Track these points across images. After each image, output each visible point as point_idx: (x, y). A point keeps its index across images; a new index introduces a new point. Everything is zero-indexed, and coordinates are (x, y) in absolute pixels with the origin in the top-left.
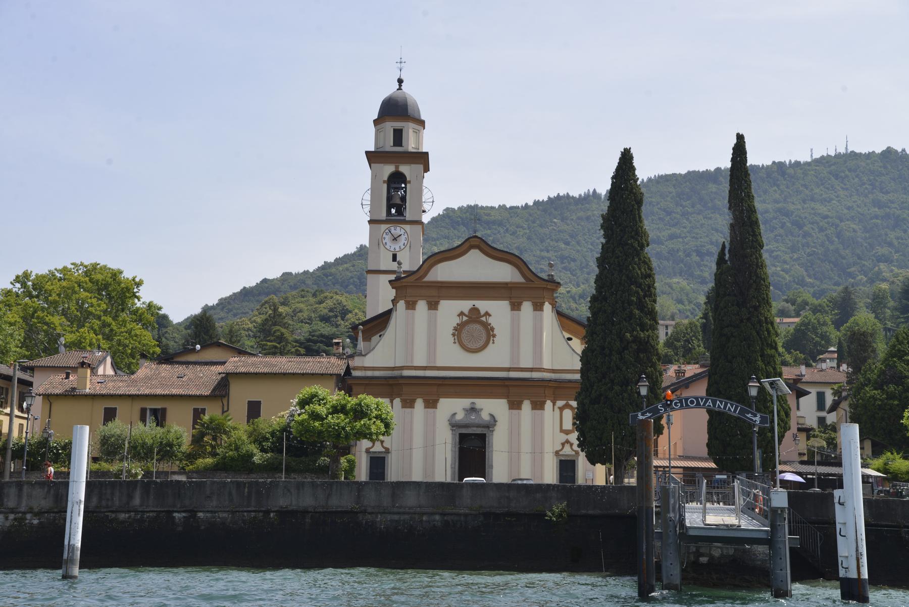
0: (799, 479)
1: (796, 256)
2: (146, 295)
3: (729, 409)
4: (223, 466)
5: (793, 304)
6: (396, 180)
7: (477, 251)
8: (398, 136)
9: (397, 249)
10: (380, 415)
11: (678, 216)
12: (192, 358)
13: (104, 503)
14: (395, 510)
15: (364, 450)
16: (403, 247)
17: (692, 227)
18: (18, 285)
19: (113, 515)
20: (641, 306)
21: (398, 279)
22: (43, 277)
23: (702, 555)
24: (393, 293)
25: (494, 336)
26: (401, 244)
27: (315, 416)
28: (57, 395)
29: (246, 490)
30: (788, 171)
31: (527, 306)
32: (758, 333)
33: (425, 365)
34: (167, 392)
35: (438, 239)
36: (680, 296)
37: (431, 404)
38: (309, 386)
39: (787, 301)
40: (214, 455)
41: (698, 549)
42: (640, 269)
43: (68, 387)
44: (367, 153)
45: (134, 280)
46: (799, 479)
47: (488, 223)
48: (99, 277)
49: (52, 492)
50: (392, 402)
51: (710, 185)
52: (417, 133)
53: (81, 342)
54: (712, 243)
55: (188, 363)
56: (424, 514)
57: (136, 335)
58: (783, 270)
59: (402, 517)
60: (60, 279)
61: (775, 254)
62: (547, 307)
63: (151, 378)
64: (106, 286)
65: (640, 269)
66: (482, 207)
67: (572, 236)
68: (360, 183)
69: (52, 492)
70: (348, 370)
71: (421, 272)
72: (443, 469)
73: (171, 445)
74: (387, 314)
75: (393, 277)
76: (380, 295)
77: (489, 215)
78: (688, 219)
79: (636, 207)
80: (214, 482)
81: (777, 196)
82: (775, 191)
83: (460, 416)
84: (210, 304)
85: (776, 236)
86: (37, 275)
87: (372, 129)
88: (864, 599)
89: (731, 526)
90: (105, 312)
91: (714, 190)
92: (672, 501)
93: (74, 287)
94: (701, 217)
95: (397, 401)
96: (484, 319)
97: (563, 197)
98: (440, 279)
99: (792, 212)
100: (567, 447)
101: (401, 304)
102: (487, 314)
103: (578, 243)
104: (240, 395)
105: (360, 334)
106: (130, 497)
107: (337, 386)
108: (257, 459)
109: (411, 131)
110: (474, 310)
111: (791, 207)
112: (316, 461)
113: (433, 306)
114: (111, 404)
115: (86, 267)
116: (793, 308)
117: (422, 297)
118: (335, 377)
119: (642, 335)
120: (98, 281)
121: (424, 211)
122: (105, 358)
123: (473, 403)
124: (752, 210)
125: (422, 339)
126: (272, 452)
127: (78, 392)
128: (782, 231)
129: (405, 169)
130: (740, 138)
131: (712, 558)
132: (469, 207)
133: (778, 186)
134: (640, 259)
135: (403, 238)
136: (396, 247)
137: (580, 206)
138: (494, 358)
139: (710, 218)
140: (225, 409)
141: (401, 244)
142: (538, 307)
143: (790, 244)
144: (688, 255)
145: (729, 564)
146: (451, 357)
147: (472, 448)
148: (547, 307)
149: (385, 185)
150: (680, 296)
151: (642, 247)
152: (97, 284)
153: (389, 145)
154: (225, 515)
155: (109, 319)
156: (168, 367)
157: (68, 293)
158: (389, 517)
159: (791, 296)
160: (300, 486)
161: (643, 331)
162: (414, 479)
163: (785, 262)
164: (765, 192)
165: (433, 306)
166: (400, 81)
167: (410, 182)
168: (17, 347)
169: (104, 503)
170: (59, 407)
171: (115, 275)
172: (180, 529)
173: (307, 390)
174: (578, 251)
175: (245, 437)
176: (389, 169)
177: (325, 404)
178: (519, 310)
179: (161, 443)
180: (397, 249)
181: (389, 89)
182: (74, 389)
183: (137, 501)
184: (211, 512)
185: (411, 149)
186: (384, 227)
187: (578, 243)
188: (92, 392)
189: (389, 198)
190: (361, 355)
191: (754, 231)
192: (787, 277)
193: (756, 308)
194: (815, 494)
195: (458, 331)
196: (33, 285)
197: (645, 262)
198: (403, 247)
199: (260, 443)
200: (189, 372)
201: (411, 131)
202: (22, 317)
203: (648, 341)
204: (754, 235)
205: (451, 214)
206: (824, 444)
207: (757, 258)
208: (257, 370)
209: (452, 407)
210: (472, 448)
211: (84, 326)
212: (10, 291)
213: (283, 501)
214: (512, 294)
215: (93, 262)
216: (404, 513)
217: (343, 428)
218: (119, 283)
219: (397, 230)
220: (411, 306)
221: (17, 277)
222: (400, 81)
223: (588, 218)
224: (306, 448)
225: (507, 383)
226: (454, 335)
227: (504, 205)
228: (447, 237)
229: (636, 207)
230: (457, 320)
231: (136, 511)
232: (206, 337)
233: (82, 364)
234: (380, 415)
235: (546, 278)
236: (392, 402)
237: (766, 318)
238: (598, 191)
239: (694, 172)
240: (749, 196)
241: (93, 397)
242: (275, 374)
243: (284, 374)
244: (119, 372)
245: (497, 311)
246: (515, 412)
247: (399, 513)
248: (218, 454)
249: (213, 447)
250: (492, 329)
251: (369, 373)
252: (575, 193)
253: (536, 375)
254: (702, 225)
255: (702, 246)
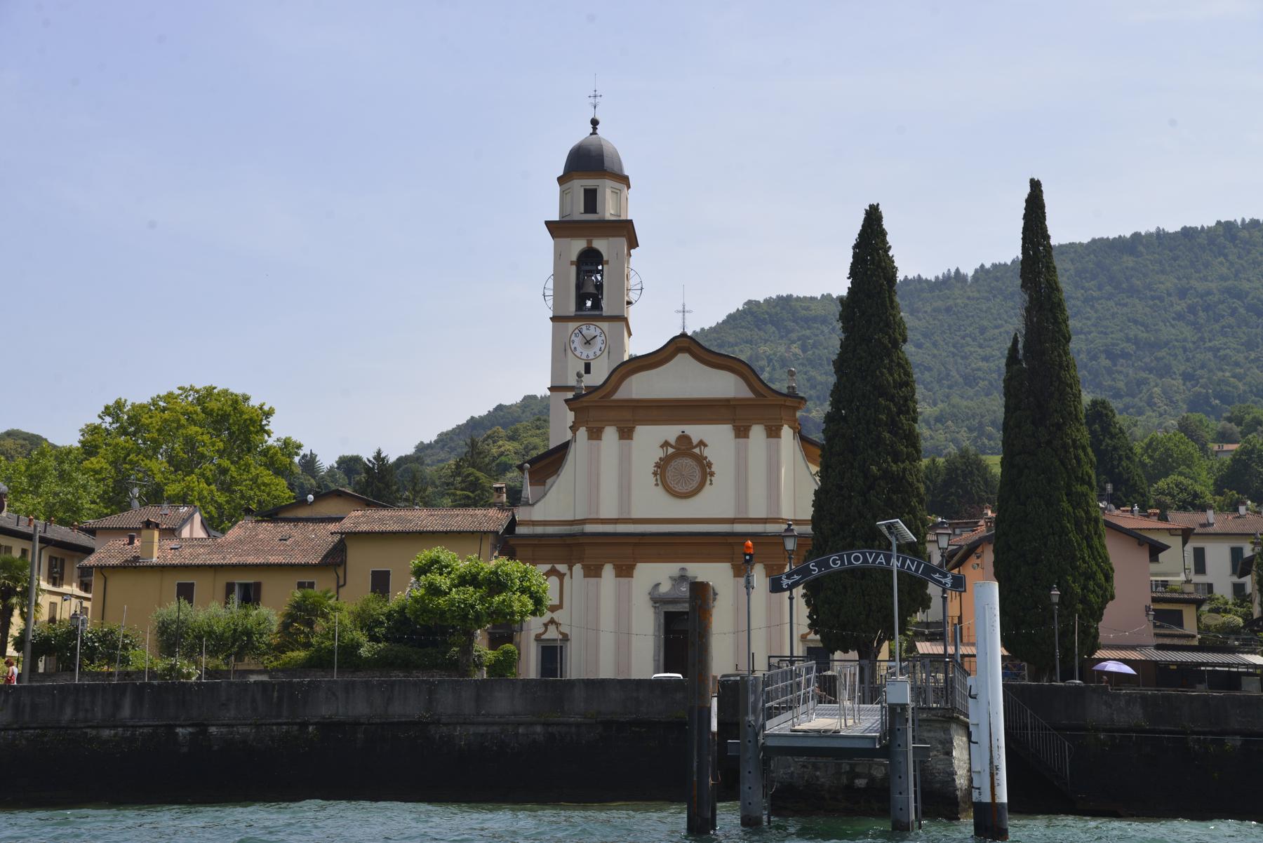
0: (1127, 669)
1: (1253, 355)
2: (278, 430)
3: (909, 567)
4: (320, 661)
5: (1239, 424)
6: (589, 261)
7: (687, 355)
8: (591, 198)
9: (592, 356)
10: (529, 588)
11: (1079, 303)
12: (303, 513)
13: (81, 715)
14: (481, 719)
15: (533, 636)
16: (598, 353)
17: (1099, 318)
18: (109, 419)
19: (94, 732)
20: (893, 426)
21: (576, 397)
22: (142, 407)
23: (859, 776)
24: (570, 416)
25: (712, 474)
26: (597, 349)
27: (434, 590)
28: (113, 567)
29: (276, 694)
30: (1241, 234)
31: (758, 432)
32: (1062, 463)
33: (764, 516)
34: (261, 560)
35: (736, 344)
36: (958, 411)
37: (625, 571)
38: (429, 548)
39: (1229, 420)
40: (307, 645)
41: (852, 766)
42: (892, 375)
43: (129, 557)
44: (547, 223)
45: (261, 408)
46: (1127, 669)
47: (806, 320)
48: (213, 405)
49: (11, 701)
50: (570, 569)
51: (1125, 258)
52: (617, 193)
53: (186, 495)
54: (1128, 340)
55: (297, 520)
56: (519, 724)
57: (265, 484)
58: (1234, 376)
59: (490, 730)
60: (164, 410)
61: (1222, 353)
62: (787, 432)
63: (250, 542)
64: (224, 417)
65: (892, 375)
66: (798, 299)
67: (925, 336)
68: (538, 265)
69: (11, 701)
70: (513, 524)
71: (609, 387)
72: (644, 662)
73: (249, 633)
74: (564, 448)
75: (570, 395)
76: (561, 424)
77: (808, 309)
78: (1092, 307)
79: (886, 287)
80: (232, 684)
81: (1225, 270)
82: (1221, 263)
83: (665, 588)
84: (426, 441)
85: (1223, 327)
86: (133, 405)
87: (556, 188)
88: (1002, 833)
89: (826, 731)
90: (221, 453)
91: (1131, 264)
92: (751, 698)
93: (179, 421)
94: (1111, 303)
95: (578, 568)
96: (697, 450)
97: (913, 281)
98: (634, 396)
99: (1247, 294)
100: (552, 628)
101: (582, 432)
102: (702, 444)
103: (935, 344)
104: (361, 563)
105: (527, 475)
106: (117, 706)
107: (495, 547)
108: (364, 651)
109: (608, 191)
110: (684, 438)
111: (1246, 286)
112: (446, 653)
113: (626, 434)
114: (186, 579)
115: (197, 392)
116: (1239, 429)
117: (611, 422)
118: (491, 539)
119: (894, 468)
120: (212, 410)
121: (629, 303)
122: (191, 516)
123: (683, 569)
124: (1054, 288)
125: (613, 480)
126: (387, 640)
127: (141, 563)
128: (1232, 320)
129: (600, 244)
130: (1036, 186)
131: (872, 779)
132: (780, 298)
133: (1226, 256)
134: (892, 361)
135: (599, 340)
136: (589, 353)
137: (937, 293)
138: (713, 505)
139: (1125, 305)
140: (341, 582)
141: (597, 349)
142: (773, 432)
143: (1245, 338)
144: (1094, 358)
145: (838, 784)
146: (652, 505)
147: (683, 629)
148: (787, 432)
149: (574, 268)
150: (958, 411)
151: (896, 345)
152: (211, 415)
153: (578, 212)
154: (247, 730)
155: (226, 463)
156: (269, 526)
157: (169, 429)
158: (472, 729)
159: (1236, 413)
160: (349, 687)
161: (895, 462)
162: (602, 676)
163: (1237, 364)
164: (1207, 265)
165: (626, 434)
166: (595, 123)
167: (607, 262)
168: (93, 502)
169: (81, 715)
170: (118, 585)
171: (237, 402)
172: (185, 750)
173: (425, 554)
174: (934, 356)
175: (347, 622)
176: (579, 245)
177: (449, 573)
178: (746, 436)
179: (235, 630)
180: (592, 356)
181: (579, 134)
182: (136, 558)
183: (126, 712)
184: (228, 725)
185: (608, 217)
186: (572, 326)
187: (935, 344)
188: (161, 562)
189: (579, 286)
190: (527, 504)
191: (1055, 318)
192: (1240, 385)
193: (1059, 427)
194: (1077, 686)
195: (662, 468)
196: (129, 418)
197: (899, 365)
198: (598, 353)
199: (370, 629)
200: (296, 532)
201: (608, 191)
202: (111, 463)
203: (904, 476)
204: (1056, 322)
205: (755, 309)
206: (1240, 621)
207: (1060, 355)
208: (383, 528)
209: (656, 575)
210: (683, 629)
211: (192, 472)
212: (96, 428)
213: (326, 710)
214: (734, 414)
215: (208, 385)
216: (493, 724)
217: (473, 607)
218: (242, 413)
219: (591, 330)
220: (595, 434)
221: (107, 408)
222: (595, 123)
223: (948, 310)
224: (424, 637)
225: (730, 540)
226: (655, 474)
227: (829, 295)
228: (750, 342)
229: (886, 287)
230: (660, 453)
231: (125, 726)
232: (381, 485)
233: (148, 524)
234: (529, 588)
235: (785, 391)
236: (570, 569)
237: (1074, 441)
238: (962, 271)
239: (1101, 240)
240: (1048, 268)
241: (163, 569)
242: (408, 533)
243: (421, 533)
244: (213, 533)
245: (716, 439)
246: (624, 580)
247: (486, 724)
248: (312, 645)
249: (307, 636)
250: (710, 465)
251: (539, 530)
252: (929, 275)
253: (621, 528)
254: (1114, 316)
255: (1113, 345)
